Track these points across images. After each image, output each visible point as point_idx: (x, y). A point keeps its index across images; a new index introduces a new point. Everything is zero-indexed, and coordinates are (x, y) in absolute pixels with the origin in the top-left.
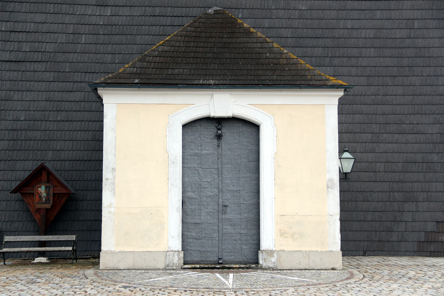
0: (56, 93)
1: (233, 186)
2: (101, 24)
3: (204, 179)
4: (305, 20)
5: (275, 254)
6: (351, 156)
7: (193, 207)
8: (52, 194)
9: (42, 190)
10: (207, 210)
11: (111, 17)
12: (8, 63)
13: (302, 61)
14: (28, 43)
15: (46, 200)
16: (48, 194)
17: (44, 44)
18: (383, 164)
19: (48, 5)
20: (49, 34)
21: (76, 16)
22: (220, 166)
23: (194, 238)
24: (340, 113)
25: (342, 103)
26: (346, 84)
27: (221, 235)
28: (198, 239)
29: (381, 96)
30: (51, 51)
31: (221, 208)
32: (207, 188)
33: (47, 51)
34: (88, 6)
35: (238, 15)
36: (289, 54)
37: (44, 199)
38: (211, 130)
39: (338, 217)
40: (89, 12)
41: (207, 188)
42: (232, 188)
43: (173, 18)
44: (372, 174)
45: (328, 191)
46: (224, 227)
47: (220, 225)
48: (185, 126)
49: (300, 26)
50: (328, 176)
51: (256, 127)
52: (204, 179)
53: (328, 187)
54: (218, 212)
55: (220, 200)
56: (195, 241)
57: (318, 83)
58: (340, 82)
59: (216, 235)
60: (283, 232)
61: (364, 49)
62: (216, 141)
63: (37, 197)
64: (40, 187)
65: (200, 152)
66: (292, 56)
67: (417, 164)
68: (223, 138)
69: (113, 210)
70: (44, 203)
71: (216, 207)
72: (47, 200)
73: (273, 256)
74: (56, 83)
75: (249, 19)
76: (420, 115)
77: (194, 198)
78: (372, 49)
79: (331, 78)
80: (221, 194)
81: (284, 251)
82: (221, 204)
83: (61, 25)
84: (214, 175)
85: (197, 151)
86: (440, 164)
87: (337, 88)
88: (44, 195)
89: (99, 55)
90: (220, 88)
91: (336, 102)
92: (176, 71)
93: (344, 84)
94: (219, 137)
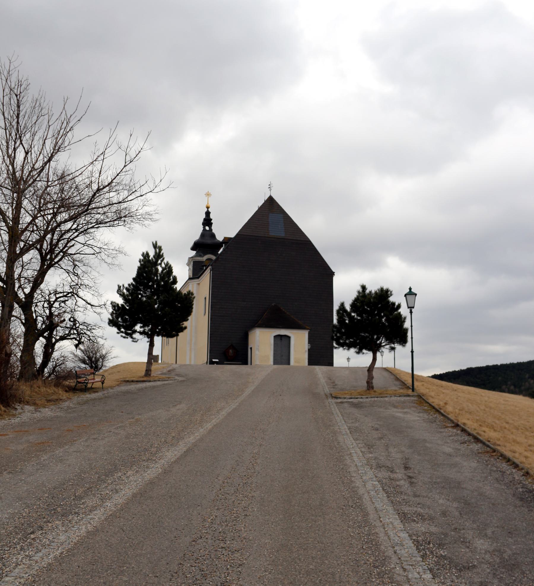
9: (231, 351)
38: (279, 338)
51: (288, 338)
94: (281, 339)
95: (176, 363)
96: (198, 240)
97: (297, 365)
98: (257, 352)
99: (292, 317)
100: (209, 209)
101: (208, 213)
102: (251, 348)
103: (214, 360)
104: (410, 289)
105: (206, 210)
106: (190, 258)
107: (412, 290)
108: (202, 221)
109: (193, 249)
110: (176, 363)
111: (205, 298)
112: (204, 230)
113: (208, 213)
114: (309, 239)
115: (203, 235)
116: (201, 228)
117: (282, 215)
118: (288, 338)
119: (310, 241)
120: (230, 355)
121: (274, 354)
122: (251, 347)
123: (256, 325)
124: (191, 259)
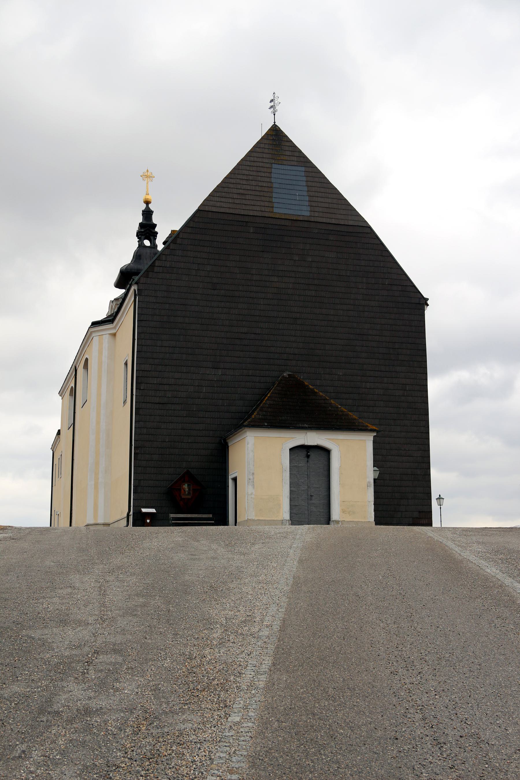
0: (187, 424)
1: (316, 485)
2: (215, 380)
3: (300, 481)
4: (342, 382)
5: (340, 523)
6: (378, 469)
7: (294, 496)
8: (191, 489)
9: (186, 486)
10: (302, 498)
11: (221, 376)
12: (158, 404)
13: (350, 413)
14: (170, 392)
15: (188, 493)
16: (189, 490)
17: (180, 392)
18: (388, 475)
19: (183, 367)
20: (183, 386)
21: (199, 375)
22: (308, 473)
23: (295, 514)
24: (374, 442)
25: (374, 437)
26: (378, 429)
27: (309, 512)
28: (297, 514)
29: (387, 432)
30: (184, 397)
31: (309, 496)
32: (301, 485)
33: (182, 397)
34: (207, 368)
35: (301, 377)
36: (342, 408)
37: (187, 492)
38: (304, 453)
39: (373, 503)
40: (208, 372)
41: (301, 485)
42: (315, 486)
43: (260, 377)
44: (382, 481)
45: (368, 488)
46: (311, 508)
47: (309, 507)
48: (291, 450)
49: (339, 386)
50: (368, 480)
51: (327, 452)
52: (300, 481)
53: (368, 486)
54: (308, 499)
55: (309, 492)
56: (296, 515)
57: (363, 428)
58: (374, 428)
59: (306, 512)
60: (344, 510)
61: (377, 402)
62: (306, 459)
63: (183, 491)
64: (184, 485)
65: (297, 465)
66: (344, 410)
67: (408, 475)
68: (310, 457)
69: (253, 496)
70: (187, 495)
71: (307, 496)
72: (189, 493)
73: (339, 524)
74: (187, 418)
75: (307, 380)
76: (410, 445)
77: (295, 491)
78: (382, 402)
79: (369, 425)
80: (309, 489)
81: (344, 521)
82: (309, 494)
83: (190, 380)
84: (305, 478)
85: (296, 464)
86: (421, 476)
87: (373, 431)
88: (187, 490)
89: (214, 400)
90: (312, 430)
91: (372, 438)
92: (283, 418)
93: (377, 429)
94: (308, 456)
95: (71, 525)
96: (129, 264)
97: (348, 518)
98: (250, 490)
99: (332, 402)
100: (150, 206)
101: (147, 214)
102: (235, 480)
103: (144, 510)
104: (440, 496)
105: (144, 206)
106: (113, 302)
107: (441, 496)
108: (136, 228)
109: (119, 284)
110: (71, 525)
111: (126, 364)
112: (141, 245)
113: (147, 214)
114: (366, 222)
115: (138, 256)
116: (135, 244)
117: (303, 169)
118: (327, 452)
119: (370, 228)
120: (183, 497)
121: (291, 492)
122: (233, 476)
123: (246, 423)
124: (115, 303)
